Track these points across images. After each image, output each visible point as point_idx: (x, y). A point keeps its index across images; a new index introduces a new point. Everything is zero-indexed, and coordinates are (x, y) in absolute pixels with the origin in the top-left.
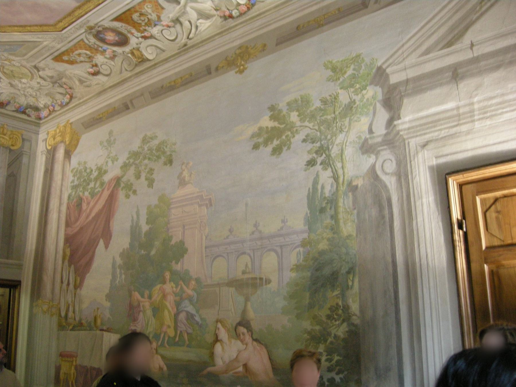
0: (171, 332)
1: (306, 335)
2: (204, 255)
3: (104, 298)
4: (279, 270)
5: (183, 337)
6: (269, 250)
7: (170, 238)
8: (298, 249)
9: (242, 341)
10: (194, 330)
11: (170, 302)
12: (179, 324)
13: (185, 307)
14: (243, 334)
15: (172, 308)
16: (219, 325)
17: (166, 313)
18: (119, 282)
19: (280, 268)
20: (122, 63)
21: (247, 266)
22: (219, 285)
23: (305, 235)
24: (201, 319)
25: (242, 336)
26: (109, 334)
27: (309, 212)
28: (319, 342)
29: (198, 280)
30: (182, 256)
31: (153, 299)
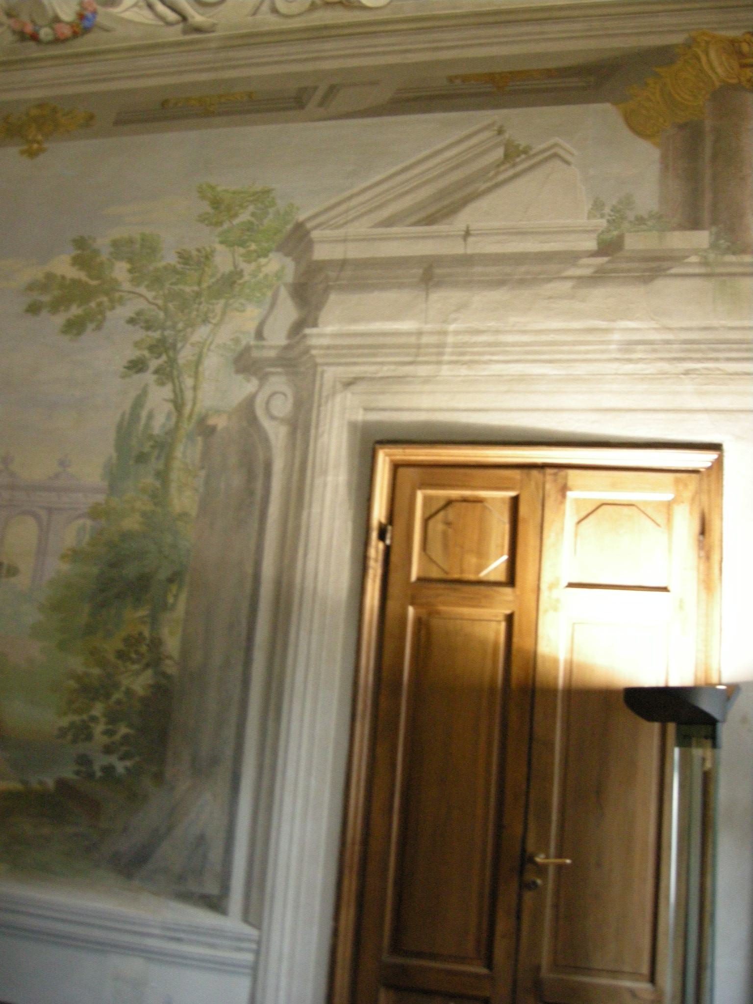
8: (81, 522)
19: (41, 552)
23: (100, 498)
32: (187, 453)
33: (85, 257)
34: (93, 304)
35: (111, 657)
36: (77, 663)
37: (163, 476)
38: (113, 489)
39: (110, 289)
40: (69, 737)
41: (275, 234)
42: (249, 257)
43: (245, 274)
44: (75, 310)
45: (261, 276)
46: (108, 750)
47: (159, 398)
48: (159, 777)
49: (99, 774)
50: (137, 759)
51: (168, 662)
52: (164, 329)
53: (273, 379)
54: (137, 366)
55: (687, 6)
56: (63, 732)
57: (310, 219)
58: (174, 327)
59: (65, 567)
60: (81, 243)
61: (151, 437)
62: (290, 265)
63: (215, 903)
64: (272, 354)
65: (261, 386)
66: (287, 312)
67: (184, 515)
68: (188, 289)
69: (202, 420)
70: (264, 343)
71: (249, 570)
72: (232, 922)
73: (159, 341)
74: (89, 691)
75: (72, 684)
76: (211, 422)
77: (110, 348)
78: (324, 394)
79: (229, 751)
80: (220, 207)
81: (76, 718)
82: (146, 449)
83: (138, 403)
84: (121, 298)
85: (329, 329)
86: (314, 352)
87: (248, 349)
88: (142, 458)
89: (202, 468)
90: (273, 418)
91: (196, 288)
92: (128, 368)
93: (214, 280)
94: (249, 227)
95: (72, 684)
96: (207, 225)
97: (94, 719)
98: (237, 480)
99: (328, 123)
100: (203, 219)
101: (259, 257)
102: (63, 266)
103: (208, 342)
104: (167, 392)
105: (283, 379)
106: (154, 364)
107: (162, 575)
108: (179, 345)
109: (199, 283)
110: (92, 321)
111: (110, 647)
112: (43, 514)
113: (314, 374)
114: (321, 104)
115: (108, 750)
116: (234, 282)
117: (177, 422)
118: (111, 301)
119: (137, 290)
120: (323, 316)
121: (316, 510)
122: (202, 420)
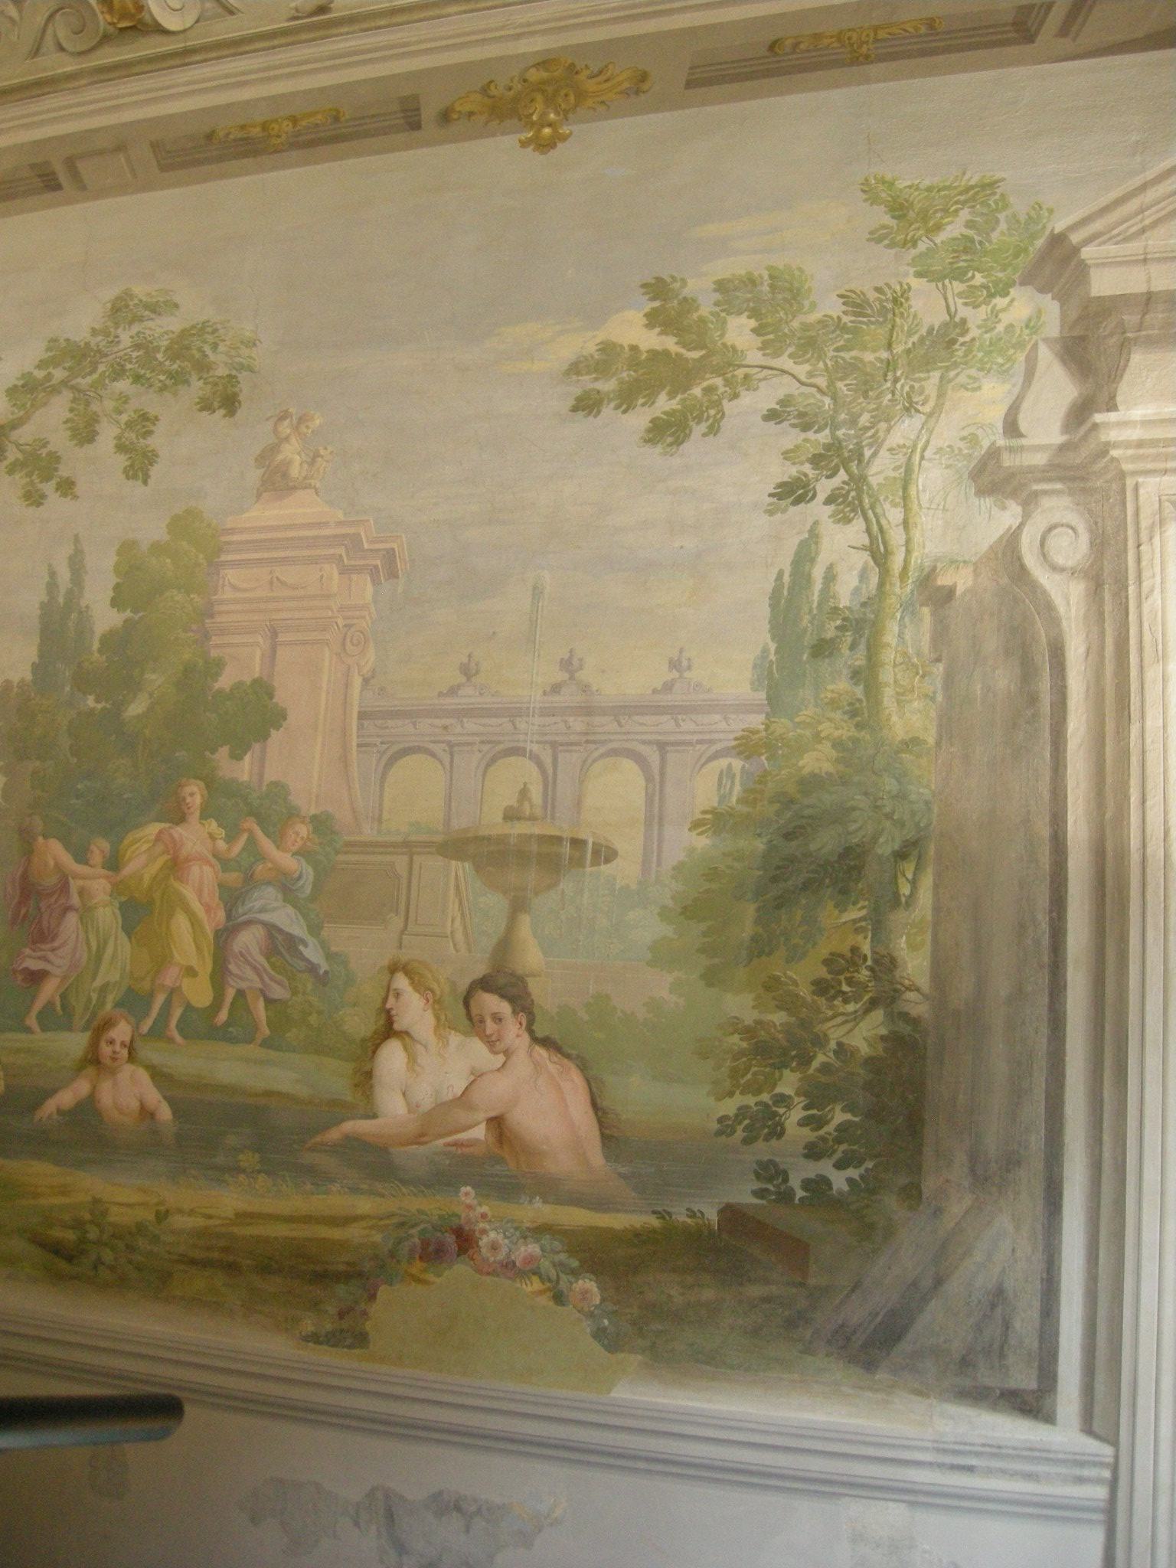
0: (199, 993)
4: (648, 823)
6: (615, 752)
7: (215, 667)
8: (723, 763)
9: (491, 1043)
10: (295, 992)
13: (262, 910)
14: (498, 1019)
15: (208, 909)
16: (401, 982)
17: (181, 923)
19: (655, 817)
20: (51, 16)
21: (524, 793)
22: (408, 847)
23: (756, 721)
24: (330, 956)
25: (490, 1026)
27: (773, 647)
29: (322, 824)
31: (127, 870)
32: (905, 637)
33: (668, 307)
34: (697, 391)
35: (805, 991)
36: (741, 1005)
37: (867, 676)
38: (775, 704)
39: (726, 362)
40: (740, 1133)
41: (1016, 256)
42: (972, 298)
43: (970, 325)
44: (664, 404)
45: (1000, 328)
46: (813, 1152)
47: (842, 546)
48: (912, 1194)
49: (800, 1193)
50: (869, 1164)
51: (911, 995)
52: (835, 427)
53: (1046, 502)
54: (794, 492)
56: (726, 1126)
57: (1074, 227)
58: (853, 421)
59: (702, 842)
60: (658, 289)
61: (835, 610)
62: (1051, 308)
63: (1033, 1404)
64: (1040, 459)
65: (1026, 516)
66: (1056, 388)
67: (912, 743)
68: (869, 357)
69: (927, 579)
70: (1024, 442)
71: (1045, 831)
72: (1064, 1434)
73: (828, 447)
74: (768, 1052)
76: (943, 580)
77: (740, 465)
78: (1144, 524)
79: (1036, 1141)
80: (906, 216)
81: (750, 1100)
82: (830, 633)
83: (805, 556)
84: (746, 376)
85: (1137, 413)
86: (1114, 453)
87: (994, 453)
88: (823, 649)
89: (938, 660)
90: (1055, 568)
91: (884, 355)
92: (779, 496)
93: (915, 338)
94: (965, 246)
96: (888, 246)
97: (782, 1099)
98: (1004, 679)
99: (1077, 63)
100: (877, 237)
101: (991, 296)
102: (632, 330)
103: (920, 446)
104: (855, 532)
105: (1066, 501)
106: (825, 487)
107: (885, 847)
108: (867, 453)
109: (889, 346)
110: (699, 420)
111: (802, 975)
112: (653, 756)
113: (1123, 491)
114: (1063, 32)
115: (813, 1152)
116: (953, 342)
117: (881, 584)
118: (728, 383)
119: (776, 363)
120: (1124, 390)
121: (1153, 721)
122: (927, 579)
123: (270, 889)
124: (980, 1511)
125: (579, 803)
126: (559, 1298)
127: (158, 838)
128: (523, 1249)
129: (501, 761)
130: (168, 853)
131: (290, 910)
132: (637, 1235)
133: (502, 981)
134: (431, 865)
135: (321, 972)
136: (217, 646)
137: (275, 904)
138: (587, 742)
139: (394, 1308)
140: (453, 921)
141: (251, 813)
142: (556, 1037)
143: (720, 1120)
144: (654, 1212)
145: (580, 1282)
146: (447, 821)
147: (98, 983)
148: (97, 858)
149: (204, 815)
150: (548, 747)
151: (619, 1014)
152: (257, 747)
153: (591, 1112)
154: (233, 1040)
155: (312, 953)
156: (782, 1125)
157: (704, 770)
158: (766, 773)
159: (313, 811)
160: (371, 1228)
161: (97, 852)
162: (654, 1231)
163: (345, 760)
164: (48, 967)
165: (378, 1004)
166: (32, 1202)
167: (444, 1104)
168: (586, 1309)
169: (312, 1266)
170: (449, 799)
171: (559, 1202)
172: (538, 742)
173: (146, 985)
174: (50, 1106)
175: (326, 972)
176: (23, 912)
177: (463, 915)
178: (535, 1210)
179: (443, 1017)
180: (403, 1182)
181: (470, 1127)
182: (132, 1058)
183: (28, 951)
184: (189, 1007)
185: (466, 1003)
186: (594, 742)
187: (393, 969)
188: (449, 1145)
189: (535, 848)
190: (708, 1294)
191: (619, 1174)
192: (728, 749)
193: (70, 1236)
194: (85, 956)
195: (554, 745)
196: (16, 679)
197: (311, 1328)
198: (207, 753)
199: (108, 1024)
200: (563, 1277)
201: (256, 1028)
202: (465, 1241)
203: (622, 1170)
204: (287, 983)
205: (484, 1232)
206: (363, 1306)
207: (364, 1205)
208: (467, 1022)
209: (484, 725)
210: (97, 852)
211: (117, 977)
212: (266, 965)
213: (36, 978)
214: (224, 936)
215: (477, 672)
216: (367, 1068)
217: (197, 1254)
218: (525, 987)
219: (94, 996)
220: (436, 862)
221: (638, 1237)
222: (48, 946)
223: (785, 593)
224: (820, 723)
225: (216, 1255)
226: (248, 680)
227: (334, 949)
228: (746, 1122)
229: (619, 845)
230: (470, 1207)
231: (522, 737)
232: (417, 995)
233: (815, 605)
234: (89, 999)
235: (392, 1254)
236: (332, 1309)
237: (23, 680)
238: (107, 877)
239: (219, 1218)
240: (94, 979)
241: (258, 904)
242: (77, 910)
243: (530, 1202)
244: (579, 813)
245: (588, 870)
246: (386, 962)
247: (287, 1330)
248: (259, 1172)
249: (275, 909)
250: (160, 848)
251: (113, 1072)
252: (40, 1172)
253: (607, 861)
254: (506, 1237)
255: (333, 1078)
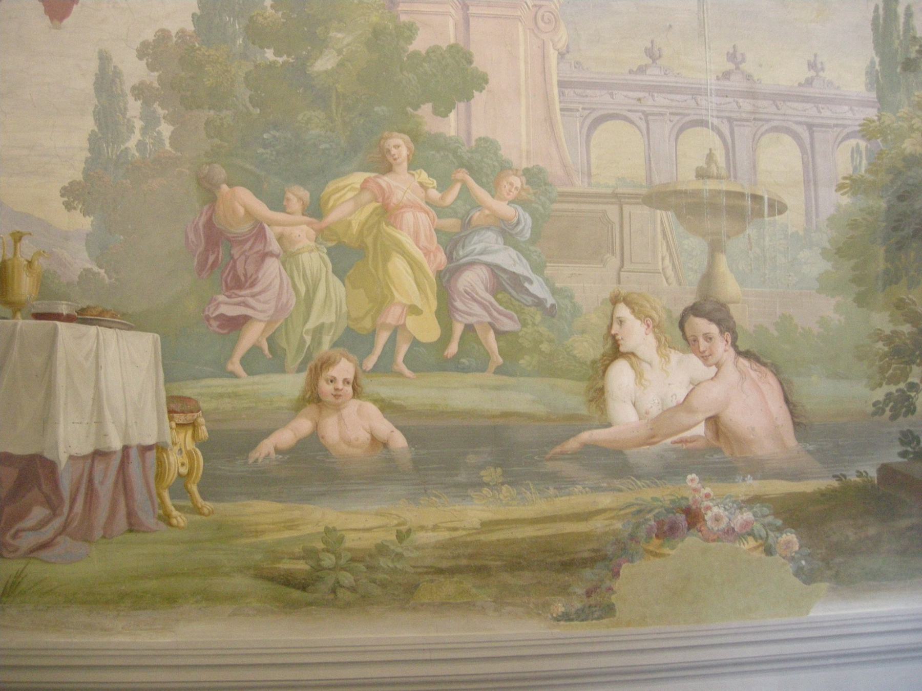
0: (426, 329)
1: (880, 345)
2: (558, 106)
3: (58, 202)
4: (807, 182)
5: (480, 343)
6: (776, 129)
7: (408, 31)
8: (853, 142)
9: (705, 358)
10: (524, 324)
11: (415, 232)
12: (458, 304)
13: (483, 252)
14: (708, 338)
15: (427, 253)
16: (623, 311)
17: (398, 266)
18: (141, 145)
19: (810, 180)
21: (710, 157)
22: (618, 198)
23: (872, 113)
24: (554, 291)
25: (703, 345)
26: (93, 330)
27: (877, 60)
28: (911, 362)
29: (534, 177)
30: (467, 97)
31: (332, 217)
40: (888, 413)
55: (463, 687)
56: (878, 408)
59: (845, 200)
75: (881, 347)
81: (893, 388)
95: (881, 347)
123: (490, 233)
124: (654, 680)
125: (754, 167)
126: (769, 551)
127: (364, 187)
128: (739, 517)
129: (689, 130)
130: (376, 200)
131: (513, 253)
132: (823, 495)
133: (708, 307)
134: (639, 213)
135: (548, 306)
136: (406, 12)
137: (496, 247)
138: (755, 119)
139: (635, 580)
140: (663, 259)
141: (462, 165)
142: (754, 350)
143: (874, 405)
144: (834, 476)
145: (784, 536)
146: (649, 178)
147: (311, 324)
148: (295, 205)
149: (412, 166)
150: (725, 121)
151: (800, 330)
152: (461, 106)
153: (785, 407)
154: (465, 370)
155: (537, 288)
156: (913, 404)
157: (842, 146)
158: (881, 153)
159: (524, 166)
160: (613, 518)
161: (294, 200)
162: (835, 490)
163: (550, 120)
164: (249, 312)
165: (604, 331)
166: (253, 540)
167: (669, 410)
168: (789, 555)
169: (559, 558)
170: (649, 160)
171: (765, 477)
172: (718, 117)
173: (367, 324)
174: (267, 447)
175: (553, 306)
176: (212, 259)
177: (671, 255)
178: (749, 486)
179: (663, 339)
180: (638, 477)
181: (690, 427)
182: (357, 392)
183: (222, 298)
184: (415, 343)
185: (682, 326)
186: (760, 120)
187: (615, 300)
188: (675, 442)
189: (724, 201)
190: (872, 531)
191: (808, 451)
192: (855, 132)
193: (302, 566)
194: (293, 301)
195: (730, 120)
196: (173, 28)
197: (561, 609)
198: (409, 109)
199: (326, 363)
200: (771, 534)
201: (488, 356)
202: (693, 517)
203: (811, 448)
204: (515, 316)
205: (708, 508)
206: (608, 583)
207: (605, 500)
208: (684, 342)
209: (672, 100)
210: (294, 200)
211: (333, 319)
212: (493, 300)
213: (236, 324)
214: (445, 281)
215: (660, 56)
216: (599, 385)
217: (445, 564)
218: (728, 312)
219: (308, 339)
220: (643, 211)
221: (825, 496)
222: (248, 292)
223: (881, 21)
224: (912, 118)
225: (464, 562)
226: (444, 46)
227: (558, 285)
228: (891, 404)
229: (788, 200)
230: (695, 490)
231: (704, 112)
232: (639, 322)
233: (901, 33)
234: (302, 341)
235: (632, 537)
236: (580, 591)
237: (182, 31)
238: (308, 224)
239: (464, 529)
240: (306, 321)
241: (479, 247)
242: (277, 256)
243: (744, 480)
244: (755, 174)
245: (767, 219)
246: (607, 295)
247: (539, 614)
248: (503, 484)
249: (496, 252)
250: (367, 196)
251: (338, 408)
252: (261, 512)
253: (780, 213)
254: (725, 509)
255: (568, 396)
